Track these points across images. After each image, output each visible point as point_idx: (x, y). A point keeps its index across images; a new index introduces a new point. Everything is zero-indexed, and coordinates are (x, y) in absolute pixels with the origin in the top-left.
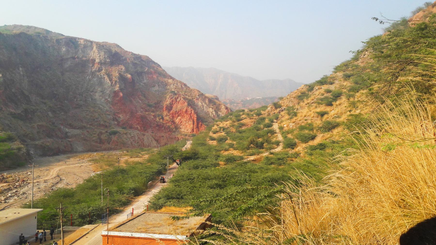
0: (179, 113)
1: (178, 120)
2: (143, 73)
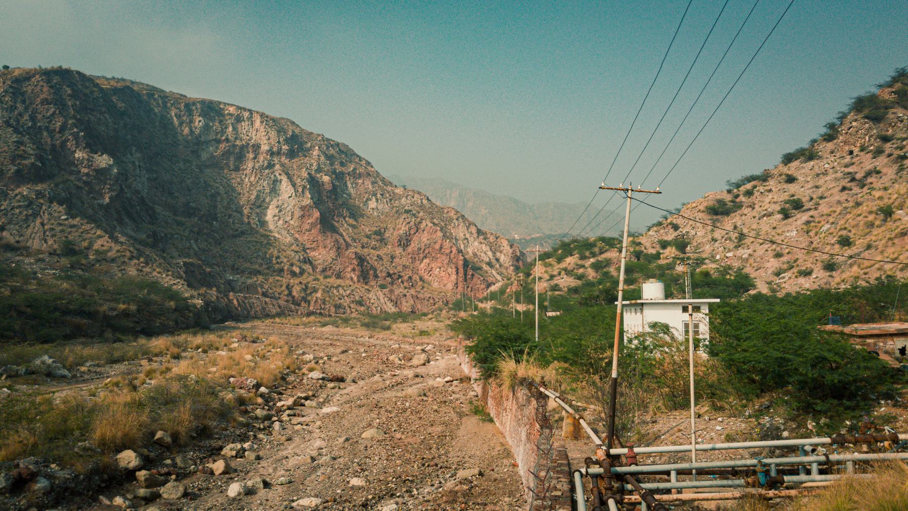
0: (424, 253)
1: (422, 265)
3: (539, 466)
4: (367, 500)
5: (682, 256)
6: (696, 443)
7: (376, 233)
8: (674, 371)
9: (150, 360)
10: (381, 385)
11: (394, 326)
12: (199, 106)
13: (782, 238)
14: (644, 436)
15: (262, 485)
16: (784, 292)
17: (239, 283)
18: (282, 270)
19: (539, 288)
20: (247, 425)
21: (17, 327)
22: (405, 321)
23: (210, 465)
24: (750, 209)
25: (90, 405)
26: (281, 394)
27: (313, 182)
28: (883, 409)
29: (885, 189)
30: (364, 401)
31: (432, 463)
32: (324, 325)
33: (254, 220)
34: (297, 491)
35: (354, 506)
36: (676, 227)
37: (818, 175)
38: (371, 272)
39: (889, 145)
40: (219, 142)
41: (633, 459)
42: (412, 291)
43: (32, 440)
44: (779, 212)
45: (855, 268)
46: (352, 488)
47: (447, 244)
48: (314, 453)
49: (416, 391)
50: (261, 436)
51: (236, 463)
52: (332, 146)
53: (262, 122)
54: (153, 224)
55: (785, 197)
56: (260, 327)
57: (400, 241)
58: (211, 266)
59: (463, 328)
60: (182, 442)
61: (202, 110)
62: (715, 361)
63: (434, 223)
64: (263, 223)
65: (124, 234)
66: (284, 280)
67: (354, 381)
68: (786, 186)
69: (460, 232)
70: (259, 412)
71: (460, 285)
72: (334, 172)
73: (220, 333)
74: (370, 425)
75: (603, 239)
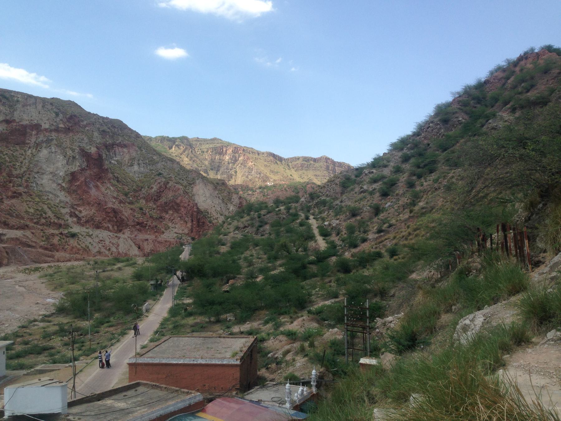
2: (114, 146)
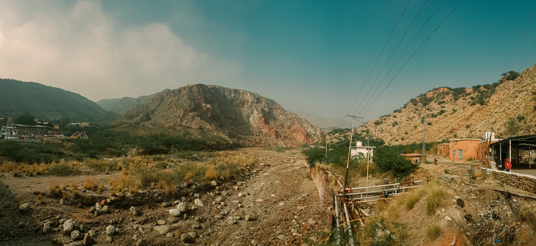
0: (295, 131)
3: (325, 194)
4: (276, 201)
5: (367, 135)
6: (368, 186)
7: (281, 125)
8: (364, 166)
9: (219, 157)
10: (281, 168)
11: (285, 151)
12: (233, 91)
13: (392, 131)
14: (354, 184)
15: (247, 194)
16: (392, 145)
17: (242, 138)
18: (254, 134)
19: (328, 142)
20: (244, 177)
21: (189, 147)
22: (288, 150)
23: (234, 187)
24: (385, 123)
25: (205, 168)
26: (253, 169)
27: (263, 110)
28: (411, 175)
29: (416, 121)
30: (276, 172)
31: (294, 192)
32: (265, 150)
33: (247, 121)
34: (257, 197)
35: (272, 202)
36: (366, 127)
37: (401, 116)
38: (279, 136)
39: (417, 111)
40: (238, 100)
41: (351, 191)
42: (291, 142)
43: (192, 175)
44: (392, 125)
45: (408, 140)
46: (272, 197)
47: (302, 129)
48: (262, 186)
49: (291, 170)
50: (247, 180)
51: (240, 187)
52: (269, 100)
53: (250, 94)
54: (220, 122)
55: (394, 121)
56: (248, 150)
57: (288, 127)
58: (235, 133)
59: (305, 153)
60: (227, 180)
61: (234, 92)
62: (374, 164)
63: (298, 123)
64: (249, 121)
65: (213, 124)
66: (254, 137)
67: (273, 166)
68: (394, 118)
69: (306, 125)
70: (247, 174)
71: (305, 140)
72: (269, 108)
73: (237, 151)
74: (277, 179)
75: (346, 129)
